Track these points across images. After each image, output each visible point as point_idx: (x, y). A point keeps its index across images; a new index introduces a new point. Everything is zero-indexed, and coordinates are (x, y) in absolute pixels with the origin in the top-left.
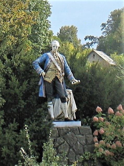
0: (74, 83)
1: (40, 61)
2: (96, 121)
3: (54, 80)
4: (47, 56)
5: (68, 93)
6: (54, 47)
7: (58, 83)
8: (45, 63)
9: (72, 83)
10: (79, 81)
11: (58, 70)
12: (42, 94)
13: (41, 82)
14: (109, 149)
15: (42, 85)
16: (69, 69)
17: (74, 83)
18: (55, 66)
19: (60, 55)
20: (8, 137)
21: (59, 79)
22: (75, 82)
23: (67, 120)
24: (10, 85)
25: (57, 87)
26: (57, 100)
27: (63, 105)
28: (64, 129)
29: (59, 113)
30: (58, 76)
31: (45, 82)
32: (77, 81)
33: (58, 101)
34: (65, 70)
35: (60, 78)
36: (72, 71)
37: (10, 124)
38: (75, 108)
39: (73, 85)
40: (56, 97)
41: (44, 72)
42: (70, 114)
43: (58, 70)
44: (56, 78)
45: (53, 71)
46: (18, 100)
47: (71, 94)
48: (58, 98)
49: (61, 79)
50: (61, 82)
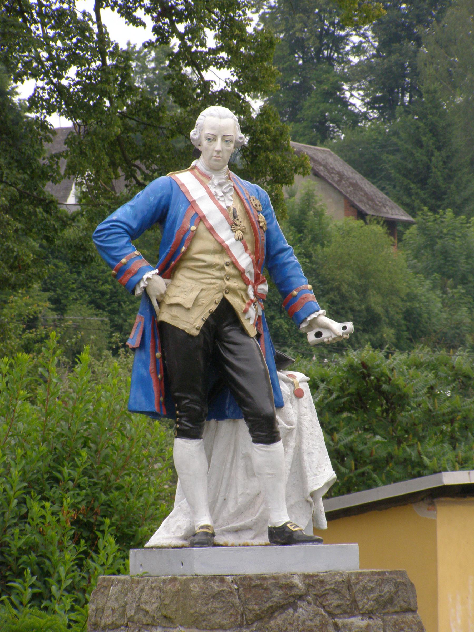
0: (319, 334)
1: (135, 218)
4: (177, 190)
5: (285, 389)
7: (235, 335)
10: (350, 325)
11: (235, 264)
13: (141, 328)
14: (49, 610)
17: (319, 334)
20: (361, 609)
21: (240, 314)
22: (326, 335)
28: (195, 588)
29: (240, 500)
30: (236, 302)
32: (336, 326)
35: (245, 312)
36: (308, 273)
39: (348, 320)
41: (159, 279)
46: (27, 284)
47: (305, 396)
48: (235, 417)
49: (250, 317)
50: (253, 332)
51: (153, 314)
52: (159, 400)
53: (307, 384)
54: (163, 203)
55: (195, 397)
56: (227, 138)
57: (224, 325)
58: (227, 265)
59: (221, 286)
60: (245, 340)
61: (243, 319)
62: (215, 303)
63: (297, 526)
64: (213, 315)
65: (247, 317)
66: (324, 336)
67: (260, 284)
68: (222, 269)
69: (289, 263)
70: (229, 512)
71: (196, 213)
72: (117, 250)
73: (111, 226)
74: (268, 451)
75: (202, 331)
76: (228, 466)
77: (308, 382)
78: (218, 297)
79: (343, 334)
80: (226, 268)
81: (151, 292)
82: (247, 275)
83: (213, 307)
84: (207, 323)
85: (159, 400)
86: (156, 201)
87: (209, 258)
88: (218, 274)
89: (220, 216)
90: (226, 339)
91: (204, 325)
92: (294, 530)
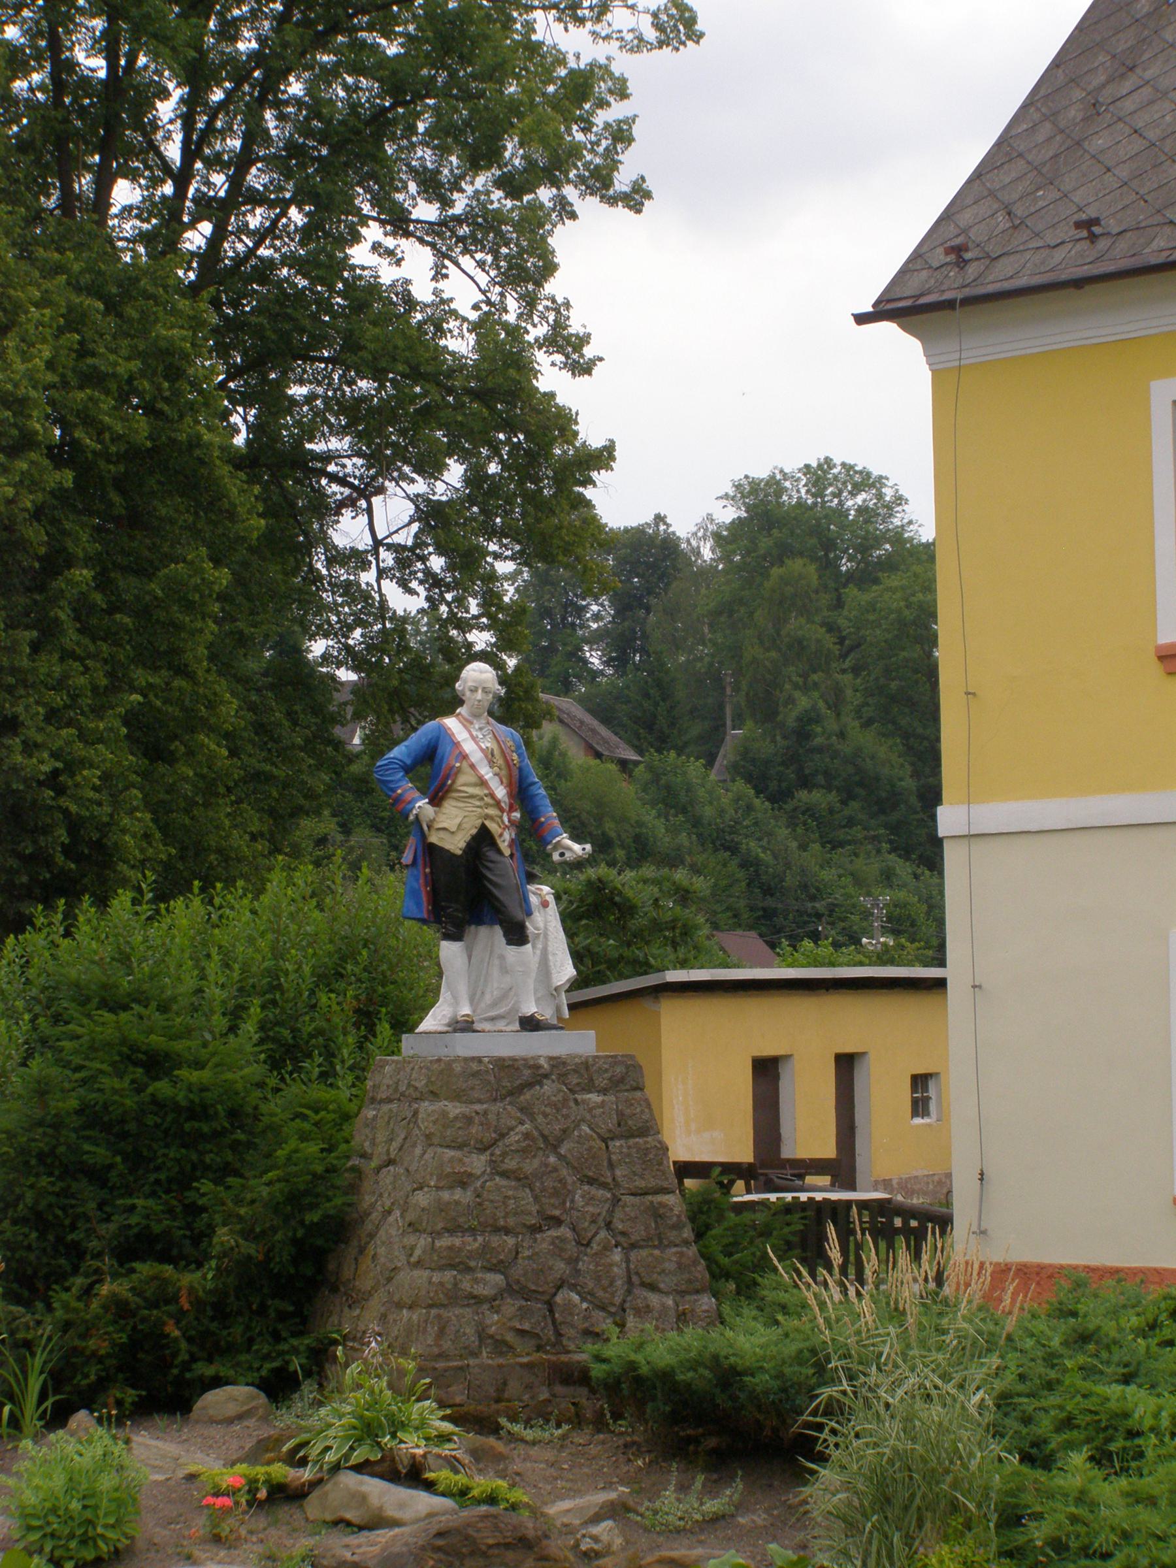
0: (562, 855)
1: (409, 755)
5: (534, 900)
7: (492, 855)
9: (556, 857)
16: (542, 791)
17: (562, 855)
22: (568, 855)
26: (483, 931)
27: (512, 952)
30: (493, 827)
32: (577, 847)
33: (492, 937)
34: (521, 793)
37: (308, 651)
38: (565, 970)
40: (479, 921)
44: (483, 838)
51: (423, 836)
61: (499, 841)
64: (475, 838)
83: (474, 831)
84: (469, 844)
89: (480, 755)
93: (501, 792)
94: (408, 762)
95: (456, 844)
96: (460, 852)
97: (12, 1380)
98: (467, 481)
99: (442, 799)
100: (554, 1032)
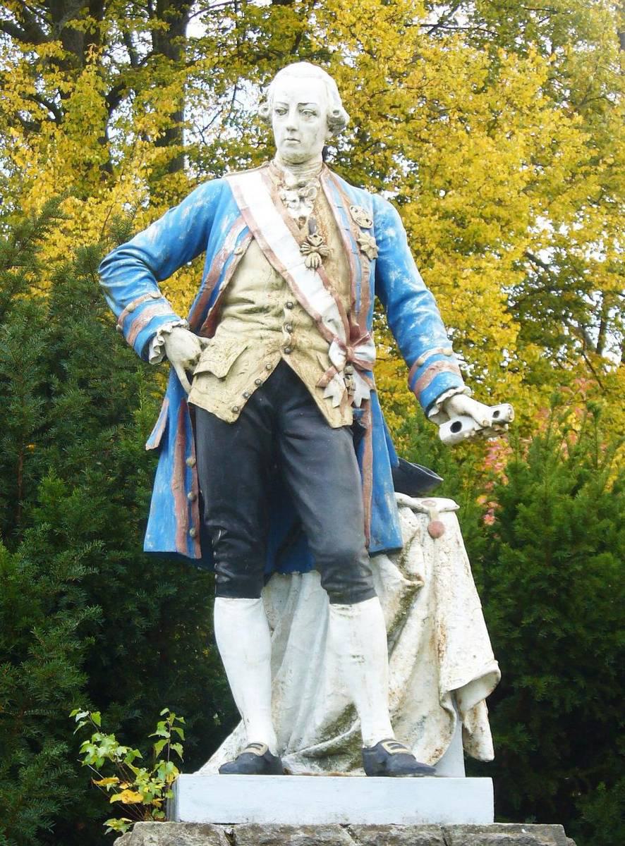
0: (456, 427)
1: (158, 244)
2: (406, 682)
3: (263, 401)
6: (283, 112)
7: (306, 427)
8: (348, 255)
12: (166, 529)
15: (174, 449)
17: (456, 427)
18: (278, 274)
19: (354, 192)
21: (312, 389)
23: (378, 764)
24: (300, 575)
25: (300, 468)
30: (307, 371)
31: (189, 414)
42: (432, 713)
43: (304, 311)
44: (283, 393)
45: (261, 317)
51: (181, 394)
52: (188, 534)
53: (454, 516)
54: (205, 216)
55: (236, 526)
56: (306, 108)
57: (286, 407)
58: (290, 308)
59: (277, 343)
60: (322, 431)
61: (318, 397)
62: (268, 370)
63: (401, 747)
64: (264, 388)
65: (326, 394)
66: (464, 429)
67: (359, 344)
68: (280, 314)
69: (418, 314)
70: (315, 724)
71: (247, 227)
72: (125, 291)
73: (120, 254)
74: (351, 617)
75: (243, 413)
76: (317, 648)
77: (456, 512)
78: (274, 361)
79: (494, 423)
80: (287, 311)
81: (173, 355)
82: (330, 327)
83: (264, 376)
84: (252, 401)
85: (188, 534)
86: (194, 214)
87: (261, 299)
88: (275, 322)
89: (284, 230)
90: (290, 432)
91: (246, 404)
92: (391, 752)
93: (322, 302)
94: (157, 253)
95: (222, 400)
96: (231, 418)
97: (504, 835)
98: (608, 310)
99: (217, 319)
100: (408, 780)
